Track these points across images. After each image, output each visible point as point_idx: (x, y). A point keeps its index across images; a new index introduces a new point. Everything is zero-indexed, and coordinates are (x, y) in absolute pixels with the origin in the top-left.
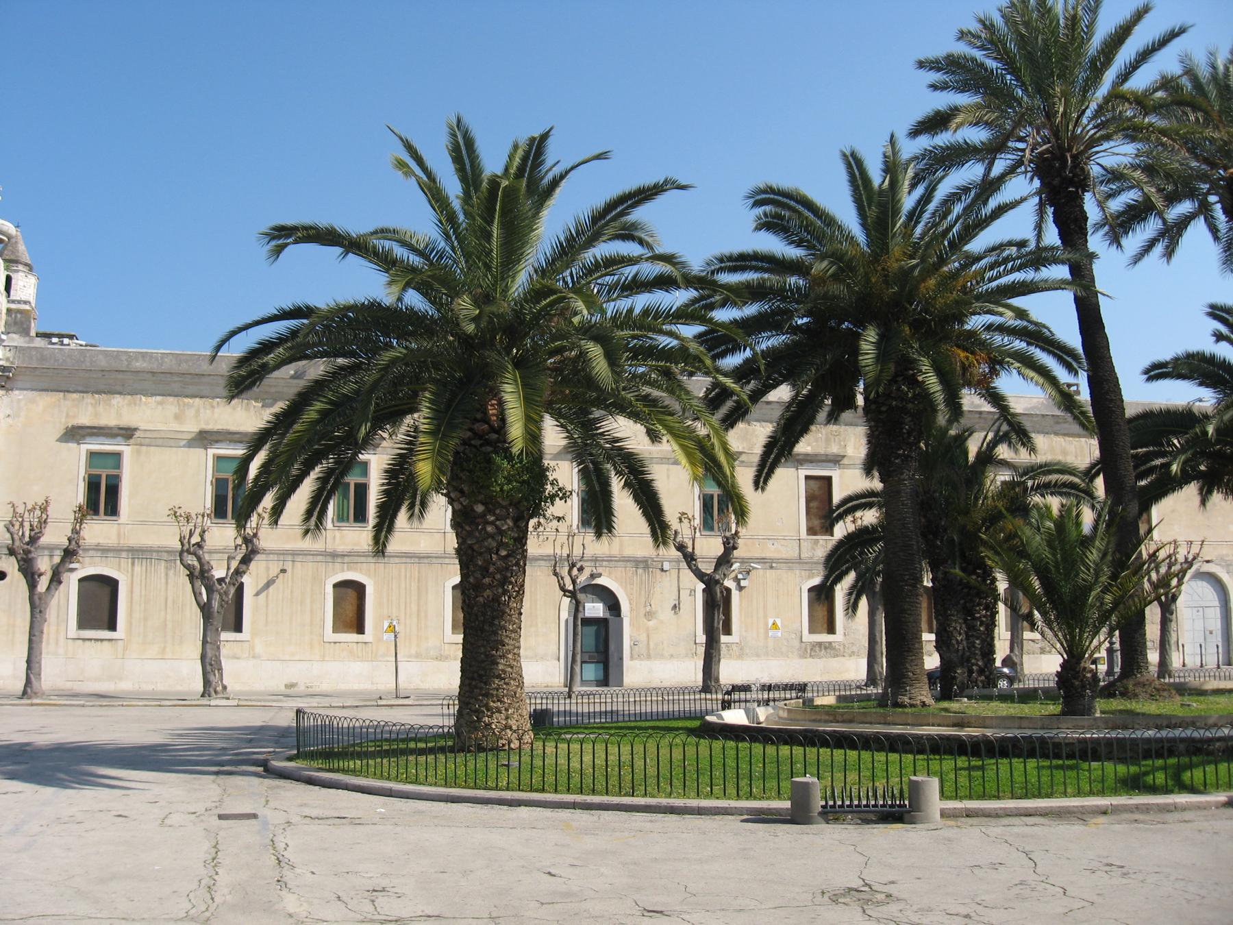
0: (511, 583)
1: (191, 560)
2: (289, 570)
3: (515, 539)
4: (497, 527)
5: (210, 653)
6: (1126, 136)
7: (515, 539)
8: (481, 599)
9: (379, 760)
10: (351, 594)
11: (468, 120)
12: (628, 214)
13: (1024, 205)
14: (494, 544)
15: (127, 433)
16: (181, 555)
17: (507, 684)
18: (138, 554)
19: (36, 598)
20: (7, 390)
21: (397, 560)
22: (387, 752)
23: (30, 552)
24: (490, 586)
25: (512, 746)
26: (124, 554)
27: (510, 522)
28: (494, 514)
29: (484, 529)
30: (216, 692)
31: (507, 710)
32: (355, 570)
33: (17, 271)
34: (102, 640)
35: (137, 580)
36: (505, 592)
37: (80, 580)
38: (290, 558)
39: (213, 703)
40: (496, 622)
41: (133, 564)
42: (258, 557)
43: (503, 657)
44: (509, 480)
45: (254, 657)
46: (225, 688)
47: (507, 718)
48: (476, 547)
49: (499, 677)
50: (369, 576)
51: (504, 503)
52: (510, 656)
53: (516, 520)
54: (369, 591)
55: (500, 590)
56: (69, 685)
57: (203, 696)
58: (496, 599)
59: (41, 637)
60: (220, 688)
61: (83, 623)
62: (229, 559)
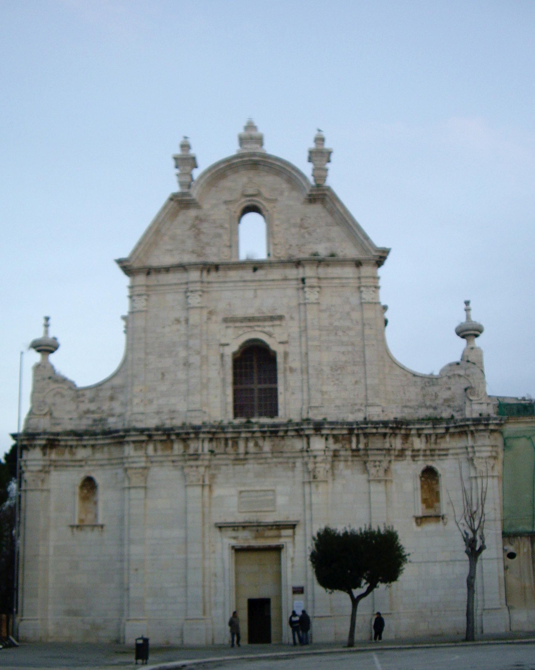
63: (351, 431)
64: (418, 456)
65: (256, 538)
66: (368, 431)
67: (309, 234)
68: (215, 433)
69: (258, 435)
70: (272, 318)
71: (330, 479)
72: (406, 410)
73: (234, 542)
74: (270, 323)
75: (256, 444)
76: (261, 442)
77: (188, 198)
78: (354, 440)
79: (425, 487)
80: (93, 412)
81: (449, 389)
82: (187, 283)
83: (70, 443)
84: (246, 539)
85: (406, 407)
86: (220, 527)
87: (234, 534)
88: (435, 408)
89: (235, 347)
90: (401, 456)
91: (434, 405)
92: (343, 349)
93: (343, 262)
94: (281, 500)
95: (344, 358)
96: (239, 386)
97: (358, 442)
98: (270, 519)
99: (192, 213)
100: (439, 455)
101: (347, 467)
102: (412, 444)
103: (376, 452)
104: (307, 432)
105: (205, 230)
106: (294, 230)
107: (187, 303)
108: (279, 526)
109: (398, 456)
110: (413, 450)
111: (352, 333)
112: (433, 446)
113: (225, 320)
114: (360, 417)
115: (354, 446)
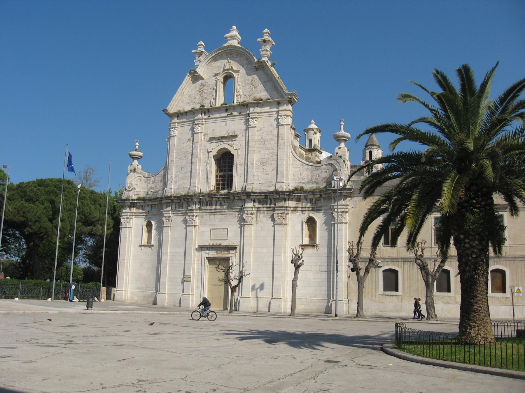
0: (479, 269)
1: (418, 261)
3: (480, 250)
4: (470, 244)
5: (429, 301)
6: (261, 100)
7: (480, 250)
8: (466, 277)
9: (416, 346)
10: (499, 275)
11: (440, 70)
12: (518, 96)
14: (470, 252)
16: (415, 260)
17: (478, 315)
19: (359, 278)
20: (352, 197)
21: (520, 259)
22: (432, 343)
23: (355, 260)
24: (469, 271)
25: (481, 343)
26: (400, 260)
27: (477, 242)
28: (469, 239)
29: (464, 245)
30: (432, 318)
31: (478, 327)
32: (500, 264)
33: (374, 149)
34: (393, 295)
35: (406, 271)
36: (476, 274)
37: (383, 271)
39: (430, 322)
40: (473, 287)
41: (404, 264)
42: (449, 260)
43: (476, 303)
44: (473, 223)
45: (456, 303)
46: (436, 316)
47: (478, 330)
48: (462, 254)
49: (474, 312)
50: (507, 267)
51: (473, 234)
52: (480, 302)
53: (480, 241)
54: (507, 274)
55: (474, 273)
56: (381, 313)
58: (472, 277)
59: (362, 294)
60: (434, 316)
61: (385, 288)
62: (435, 261)
63: (266, 197)
66: (275, 197)
69: (221, 199)
73: (207, 256)
77: (463, 70)
79: (311, 228)
80: (153, 188)
83: (141, 204)
88: (317, 183)
89: (215, 153)
90: (295, 211)
92: (267, 151)
95: (267, 156)
96: (230, 173)
98: (224, 244)
99: (200, 82)
101: (264, 217)
104: (243, 198)
105: (205, 91)
111: (272, 142)
114: (272, 189)
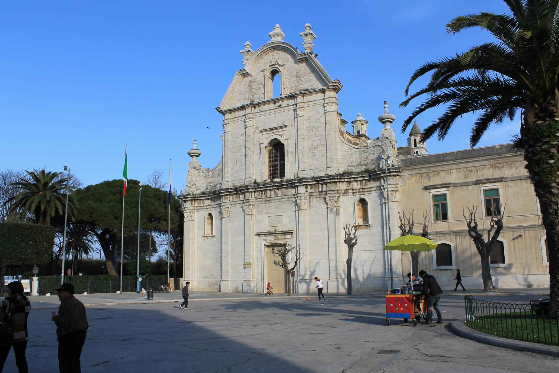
2: (523, 235)
13: (418, 91)
15: (447, 186)
16: (469, 232)
18: (457, 233)
26: (452, 234)
30: (490, 289)
34: (447, 270)
38: (523, 229)
57: (484, 291)
60: (491, 287)
64: (356, 192)
65: (275, 240)
67: (301, 80)
68: (258, 187)
70: (281, 127)
71: (308, 209)
72: (350, 168)
73: (265, 242)
74: (282, 130)
75: (275, 192)
76: (277, 191)
78: (320, 186)
81: (374, 154)
82: (245, 115)
84: (270, 240)
85: (350, 166)
86: (259, 235)
87: (265, 238)
89: (266, 143)
91: (366, 163)
93: (314, 91)
94: (286, 220)
95: (316, 143)
97: (322, 188)
98: (279, 230)
99: (249, 79)
100: (367, 191)
101: (317, 201)
102: (353, 186)
103: (330, 192)
106: (293, 79)
107: (245, 125)
108: (284, 233)
109: (344, 193)
110: (353, 190)
111: (320, 129)
112: (364, 187)
113: (261, 132)
114: (323, 174)
115: (320, 190)
